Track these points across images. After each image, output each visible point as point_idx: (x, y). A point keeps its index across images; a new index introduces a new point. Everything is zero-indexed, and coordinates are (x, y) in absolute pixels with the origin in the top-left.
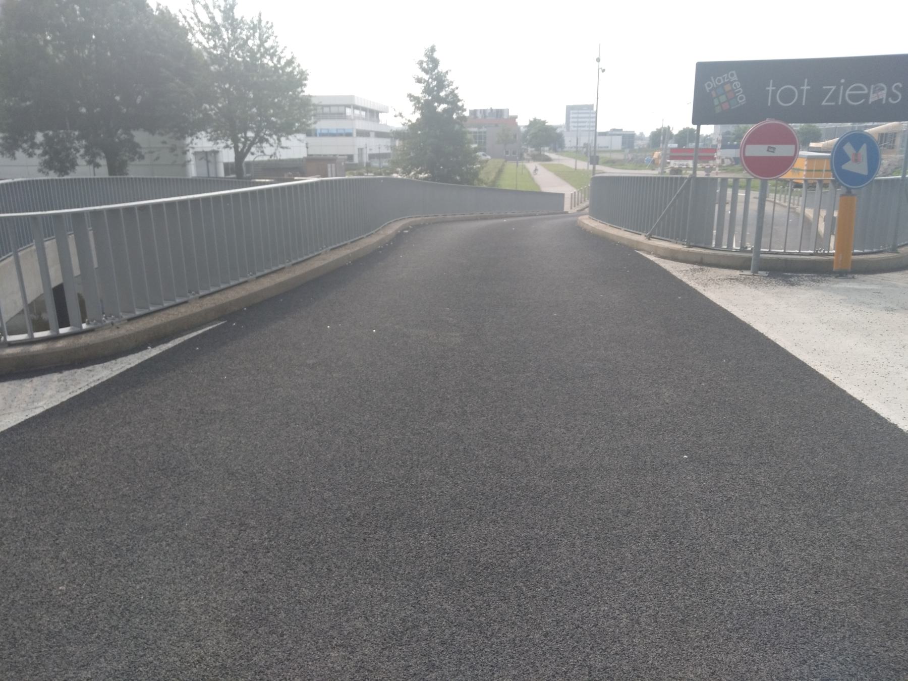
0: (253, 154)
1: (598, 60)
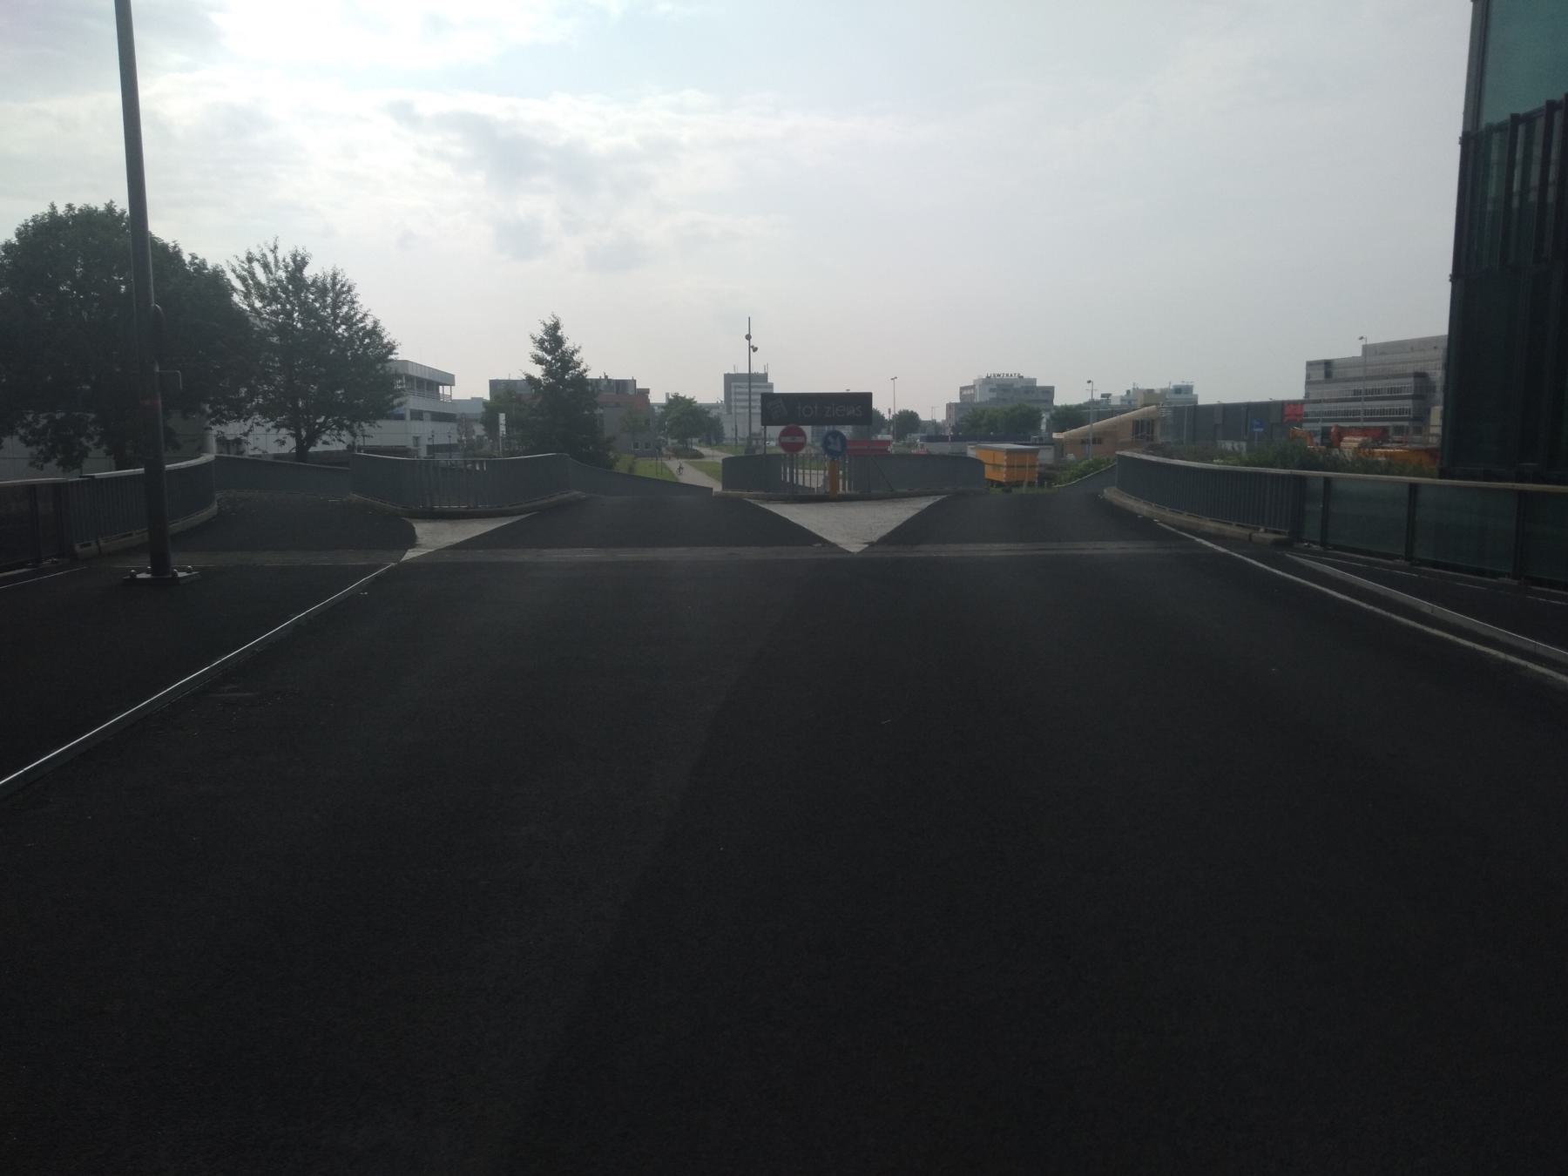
0: (325, 443)
1: (748, 337)
